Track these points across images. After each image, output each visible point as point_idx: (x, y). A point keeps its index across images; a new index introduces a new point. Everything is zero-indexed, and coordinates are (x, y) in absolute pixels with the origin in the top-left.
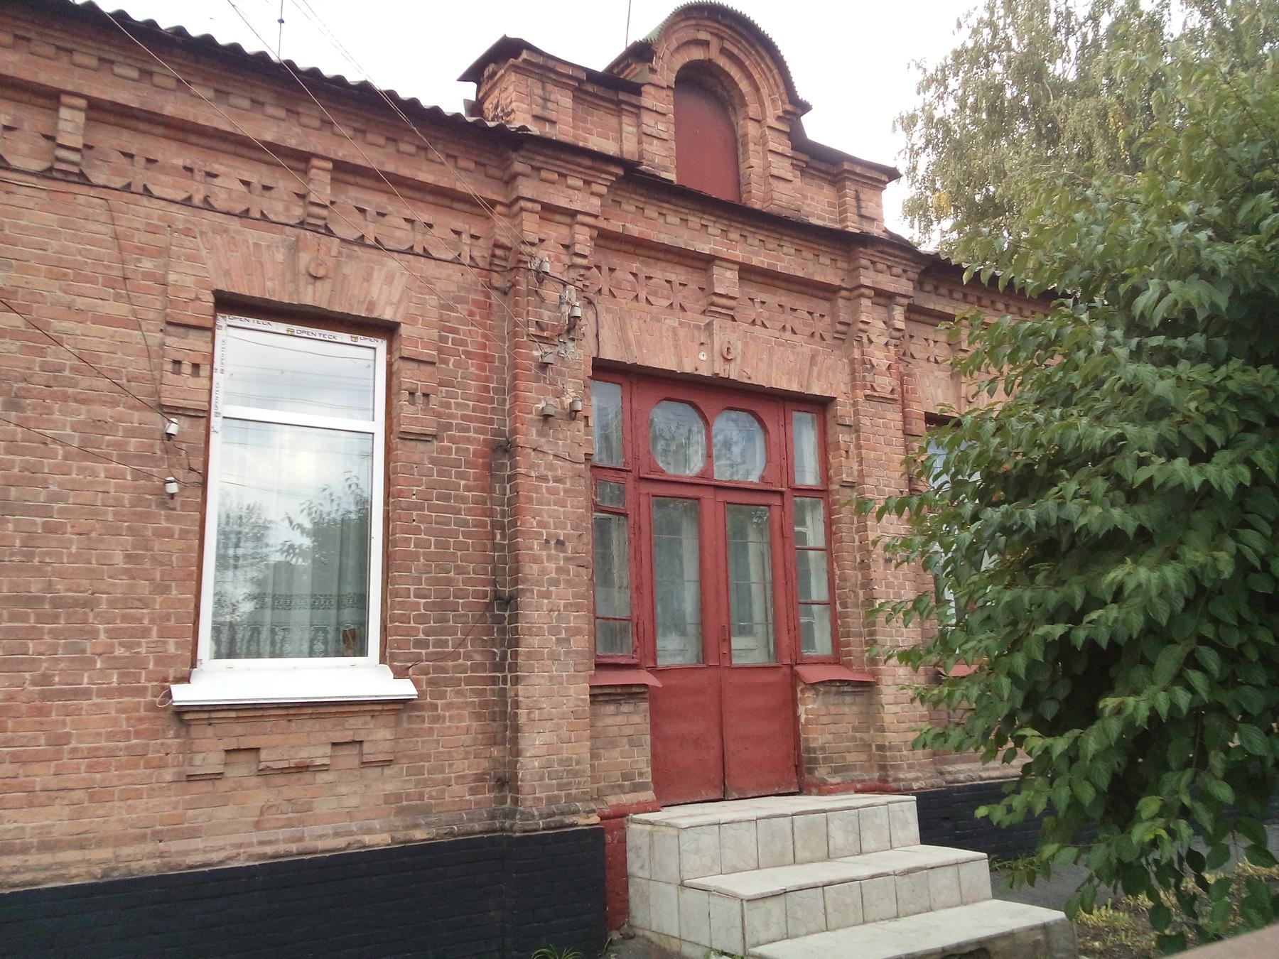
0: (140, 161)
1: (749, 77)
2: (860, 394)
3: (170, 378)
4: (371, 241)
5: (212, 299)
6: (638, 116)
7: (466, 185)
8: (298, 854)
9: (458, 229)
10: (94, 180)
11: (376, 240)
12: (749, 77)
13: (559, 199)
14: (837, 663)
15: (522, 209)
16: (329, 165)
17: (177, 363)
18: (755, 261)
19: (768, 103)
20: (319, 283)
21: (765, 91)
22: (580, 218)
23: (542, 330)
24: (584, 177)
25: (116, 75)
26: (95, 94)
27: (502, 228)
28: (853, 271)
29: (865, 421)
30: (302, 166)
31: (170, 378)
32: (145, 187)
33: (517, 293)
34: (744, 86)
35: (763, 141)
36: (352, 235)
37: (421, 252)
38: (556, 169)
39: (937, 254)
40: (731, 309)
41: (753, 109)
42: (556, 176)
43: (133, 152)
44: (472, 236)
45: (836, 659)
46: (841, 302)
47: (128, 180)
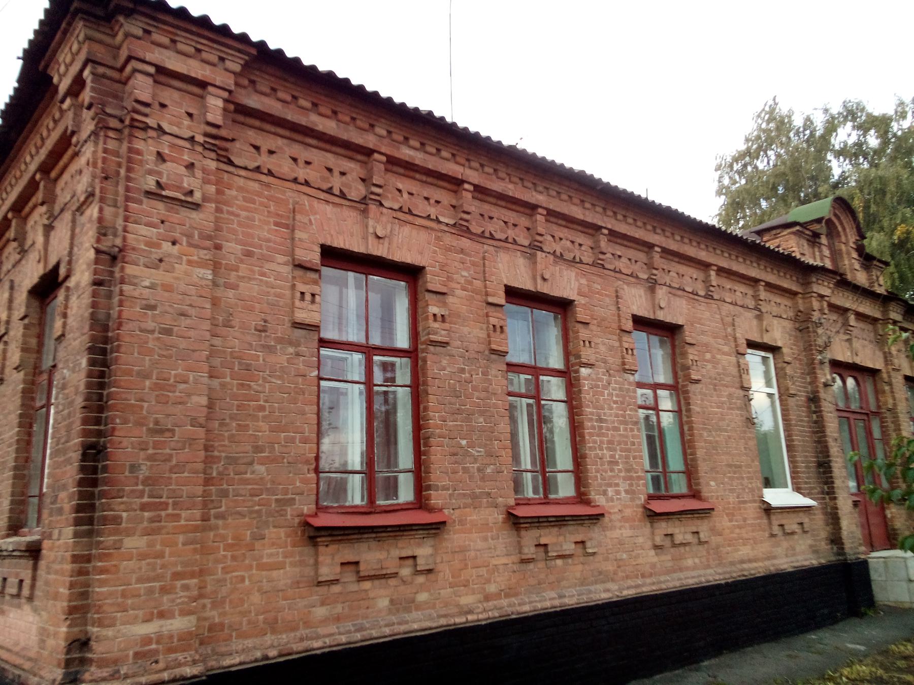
0: (336, 173)
1: (842, 224)
2: (890, 367)
3: (298, 303)
4: (434, 217)
5: (319, 250)
6: (819, 248)
7: (786, 284)
8: (362, 641)
9: (258, 144)
10: (545, 249)
11: (341, 191)
12: (842, 224)
13: (174, 63)
14: (420, 508)
15: (135, 70)
16: (384, 159)
17: (302, 293)
18: (617, 229)
19: (849, 237)
20: (381, 241)
21: (848, 230)
22: (210, 89)
23: (163, 189)
24: (219, 54)
25: (394, 141)
26: (551, 207)
27: (801, 304)
28: (885, 312)
29: (894, 380)
30: (454, 188)
31: (298, 303)
32: (514, 240)
33: (809, 332)
34: (840, 228)
35: (849, 253)
36: (478, 230)
37: (407, 211)
38: (193, 44)
39: (742, 237)
40: (379, 195)
41: (843, 239)
42: (193, 50)
43: (414, 192)
44: (411, 194)
45: (371, 508)
46: (879, 326)
47: (330, 185)
